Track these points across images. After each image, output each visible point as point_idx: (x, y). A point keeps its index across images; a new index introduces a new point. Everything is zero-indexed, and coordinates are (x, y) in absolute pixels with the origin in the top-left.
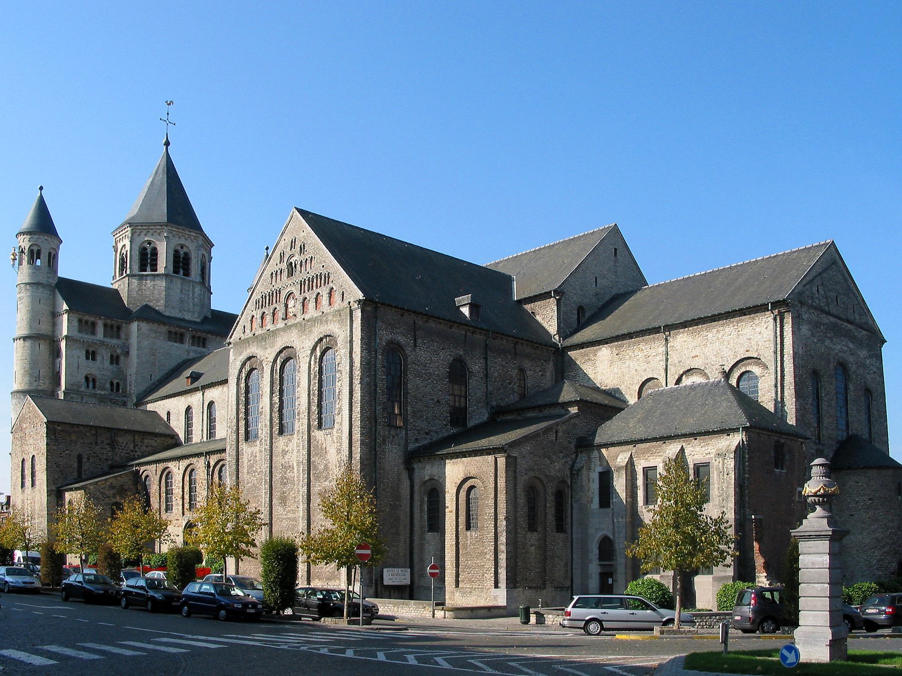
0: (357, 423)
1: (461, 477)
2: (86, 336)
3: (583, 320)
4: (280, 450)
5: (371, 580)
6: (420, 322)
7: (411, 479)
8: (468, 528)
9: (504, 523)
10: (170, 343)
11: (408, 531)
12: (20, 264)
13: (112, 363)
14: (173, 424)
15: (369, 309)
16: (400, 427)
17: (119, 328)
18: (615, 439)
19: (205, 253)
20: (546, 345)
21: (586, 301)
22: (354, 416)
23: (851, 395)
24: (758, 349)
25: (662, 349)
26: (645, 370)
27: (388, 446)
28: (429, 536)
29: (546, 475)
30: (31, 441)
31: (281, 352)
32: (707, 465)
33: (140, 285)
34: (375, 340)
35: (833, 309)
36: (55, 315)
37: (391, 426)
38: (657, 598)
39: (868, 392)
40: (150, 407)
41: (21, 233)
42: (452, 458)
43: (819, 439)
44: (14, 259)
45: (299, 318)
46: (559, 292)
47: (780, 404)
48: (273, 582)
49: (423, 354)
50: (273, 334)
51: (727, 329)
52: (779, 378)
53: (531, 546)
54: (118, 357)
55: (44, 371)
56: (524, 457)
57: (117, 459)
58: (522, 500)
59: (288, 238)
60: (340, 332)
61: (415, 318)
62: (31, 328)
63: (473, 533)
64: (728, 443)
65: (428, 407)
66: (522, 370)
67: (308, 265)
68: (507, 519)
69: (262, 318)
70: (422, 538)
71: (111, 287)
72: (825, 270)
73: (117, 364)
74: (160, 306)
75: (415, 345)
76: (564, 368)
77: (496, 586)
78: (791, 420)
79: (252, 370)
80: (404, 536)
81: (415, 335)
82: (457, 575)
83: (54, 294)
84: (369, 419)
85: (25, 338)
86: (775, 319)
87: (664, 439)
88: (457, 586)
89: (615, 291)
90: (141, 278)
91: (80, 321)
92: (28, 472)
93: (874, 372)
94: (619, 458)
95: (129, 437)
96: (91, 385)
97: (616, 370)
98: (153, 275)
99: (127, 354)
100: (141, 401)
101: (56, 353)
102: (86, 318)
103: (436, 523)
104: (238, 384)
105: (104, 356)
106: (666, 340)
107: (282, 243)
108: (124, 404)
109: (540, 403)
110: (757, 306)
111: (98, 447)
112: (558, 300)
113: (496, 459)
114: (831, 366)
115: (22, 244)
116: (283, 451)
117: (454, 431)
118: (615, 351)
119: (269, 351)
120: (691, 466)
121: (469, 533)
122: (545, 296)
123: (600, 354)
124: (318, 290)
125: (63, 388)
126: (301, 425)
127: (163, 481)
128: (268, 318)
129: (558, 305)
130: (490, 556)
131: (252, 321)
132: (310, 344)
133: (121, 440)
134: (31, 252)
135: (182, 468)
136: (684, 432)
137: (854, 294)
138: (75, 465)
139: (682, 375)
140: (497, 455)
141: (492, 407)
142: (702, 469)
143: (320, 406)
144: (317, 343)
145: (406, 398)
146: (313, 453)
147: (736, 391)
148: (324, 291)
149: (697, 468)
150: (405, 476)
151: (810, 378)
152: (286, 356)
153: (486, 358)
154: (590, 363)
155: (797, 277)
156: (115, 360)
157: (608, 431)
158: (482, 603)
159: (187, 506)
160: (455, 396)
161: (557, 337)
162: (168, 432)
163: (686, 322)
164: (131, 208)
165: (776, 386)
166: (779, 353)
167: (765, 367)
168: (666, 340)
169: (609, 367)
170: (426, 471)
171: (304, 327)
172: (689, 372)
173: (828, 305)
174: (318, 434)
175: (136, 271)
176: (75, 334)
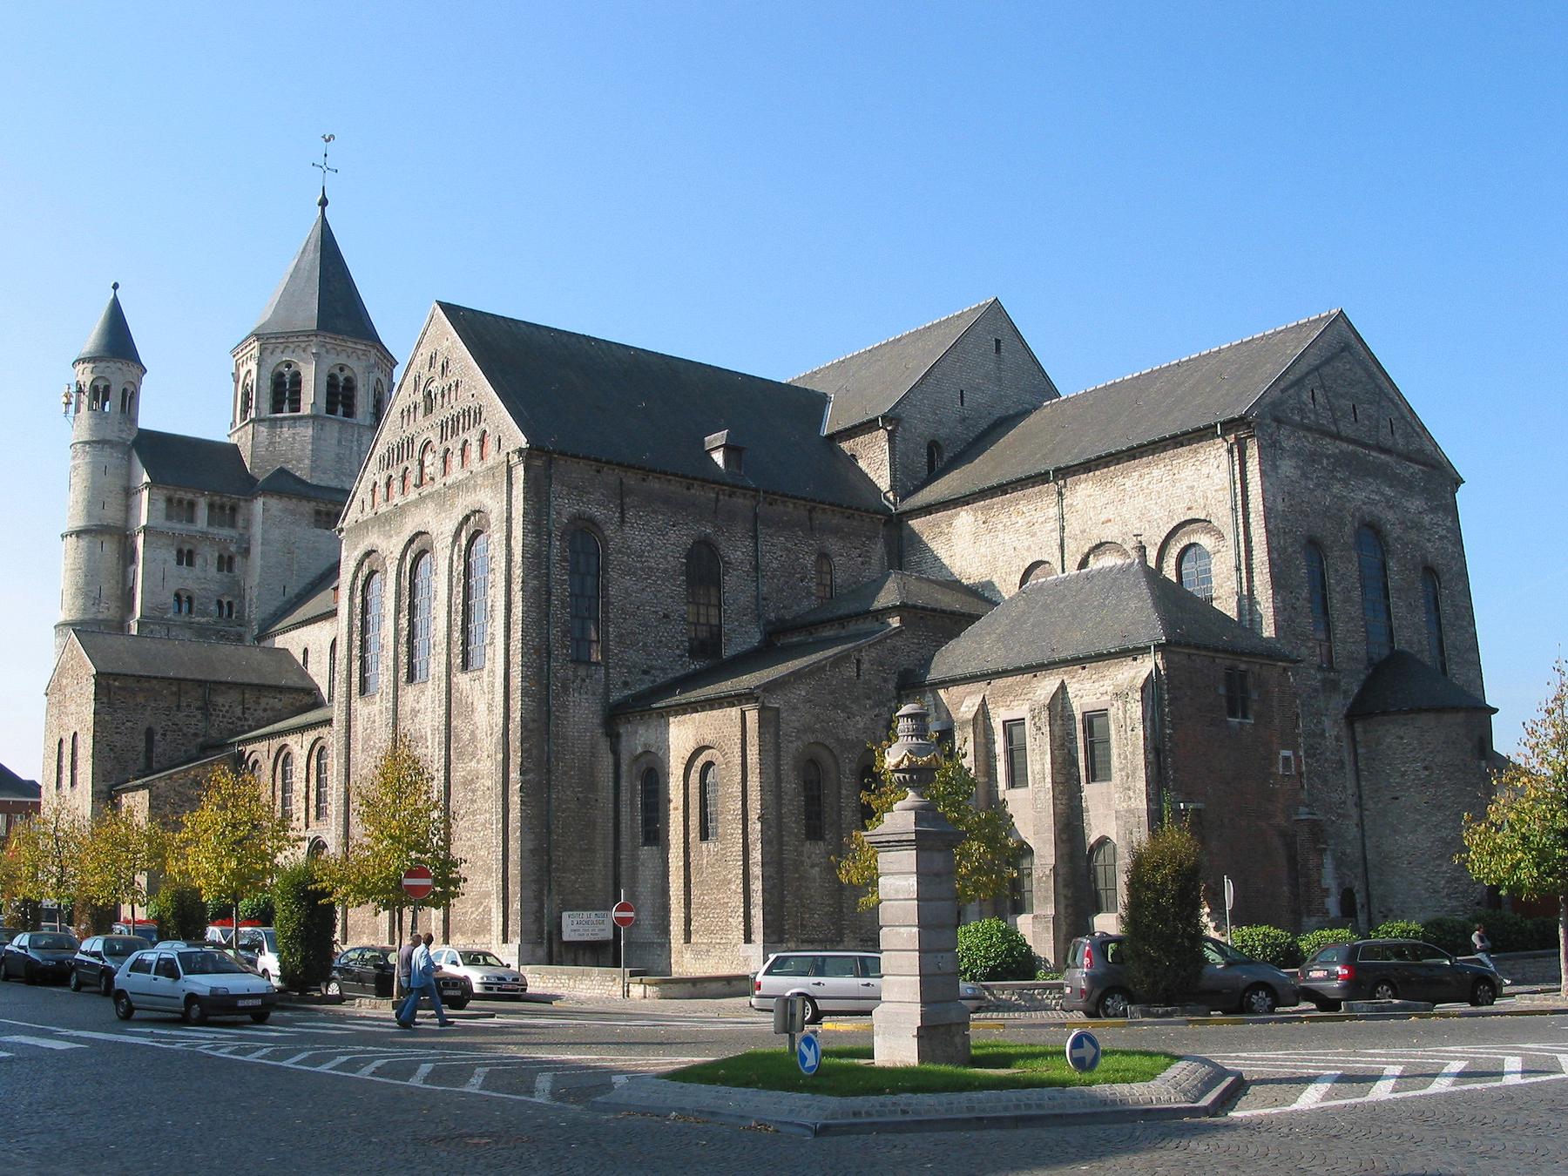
0: (517, 659)
1: (691, 746)
2: (178, 526)
3: (939, 465)
4: (408, 709)
5: (540, 932)
6: (631, 480)
7: (616, 752)
8: (704, 836)
9: (758, 826)
10: (318, 531)
11: (611, 846)
12: (77, 410)
13: (220, 569)
14: (312, 670)
15: (538, 463)
16: (597, 664)
17: (234, 509)
18: (958, 672)
19: (382, 377)
20: (867, 511)
21: (943, 432)
22: (512, 648)
23: (1394, 579)
24: (1199, 507)
25: (1053, 511)
26: (1029, 547)
27: (574, 697)
28: (645, 852)
29: (838, 740)
30: (73, 708)
31: (411, 541)
32: (1103, 713)
33: (271, 435)
34: (548, 514)
35: (1347, 428)
36: (129, 492)
37: (581, 660)
38: (997, 956)
39: (1430, 572)
40: (280, 642)
41: (79, 361)
42: (676, 714)
43: (1330, 661)
44: (68, 404)
45: (438, 485)
46: (892, 421)
47: (1247, 601)
48: (291, 938)
49: (637, 536)
50: (400, 511)
51: (1156, 472)
52: (1243, 554)
53: (813, 866)
54: (231, 559)
55: (109, 587)
56: (795, 708)
57: (214, 733)
58: (791, 785)
59: (425, 352)
60: (491, 501)
61: (622, 474)
62: (89, 515)
63: (711, 846)
64: (1132, 673)
65: (645, 625)
66: (824, 556)
67: (453, 393)
68: (761, 818)
69: (388, 485)
70: (634, 857)
71: (228, 440)
72: (1328, 361)
73: (230, 570)
74: (302, 470)
75: (623, 521)
76: (902, 549)
77: (748, 939)
78: (1268, 631)
79: (372, 573)
80: (603, 856)
81: (622, 504)
82: (688, 922)
83: (130, 457)
84: (537, 651)
85: (79, 533)
86: (1230, 451)
87: (1035, 669)
88: (688, 939)
89: (998, 413)
90: (273, 423)
91: (169, 500)
92: (66, 762)
93: (1442, 538)
94: (963, 704)
95: (234, 695)
96: (185, 607)
97: (983, 550)
98: (294, 418)
99: (246, 552)
100: (265, 634)
101: (128, 556)
102: (180, 494)
103: (655, 834)
104: (351, 599)
105: (207, 557)
106: (1060, 494)
107: (418, 359)
108: (240, 639)
109: (840, 612)
110: (1199, 430)
111: (180, 715)
112: (890, 433)
113: (743, 713)
114: (1348, 529)
115: (82, 379)
116: (413, 710)
117: (696, 666)
118: (981, 518)
119: (394, 540)
120: (1079, 717)
121: (704, 845)
122: (868, 426)
123: (957, 522)
124: (466, 436)
125: (138, 615)
126: (435, 664)
127: (314, 763)
128: (396, 485)
129: (891, 439)
130: (737, 886)
131: (373, 490)
132: (450, 526)
133: (220, 700)
134: (95, 389)
135: (307, 746)
136: (1063, 655)
137: (1392, 401)
138: (142, 746)
139: (1088, 556)
140: (745, 707)
141: (769, 622)
142: (1095, 721)
143: (465, 631)
144: (461, 525)
145: (606, 612)
146: (454, 712)
147: (1154, 576)
148: (473, 436)
149: (1090, 719)
150: (604, 746)
151: (1300, 552)
152: (418, 549)
153: (755, 538)
154: (943, 538)
155: (1271, 376)
156: (226, 563)
157: (954, 656)
158: (725, 970)
159: (313, 812)
160: (698, 604)
161: (891, 496)
162: (301, 684)
163: (1089, 461)
164: (259, 308)
165: (1238, 569)
166: (1240, 510)
167: (1221, 536)
168: (1060, 494)
169: (975, 544)
170: (637, 737)
171: (443, 498)
172: (1098, 548)
173: (1335, 422)
174: (462, 680)
175: (266, 412)
176: (161, 523)
